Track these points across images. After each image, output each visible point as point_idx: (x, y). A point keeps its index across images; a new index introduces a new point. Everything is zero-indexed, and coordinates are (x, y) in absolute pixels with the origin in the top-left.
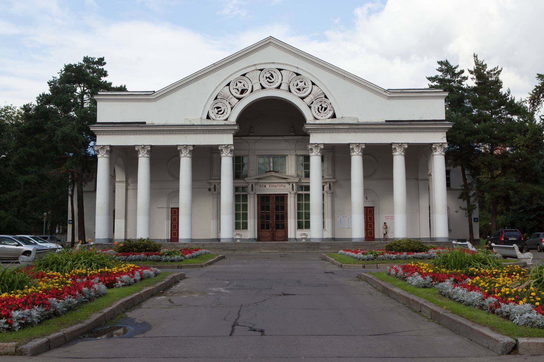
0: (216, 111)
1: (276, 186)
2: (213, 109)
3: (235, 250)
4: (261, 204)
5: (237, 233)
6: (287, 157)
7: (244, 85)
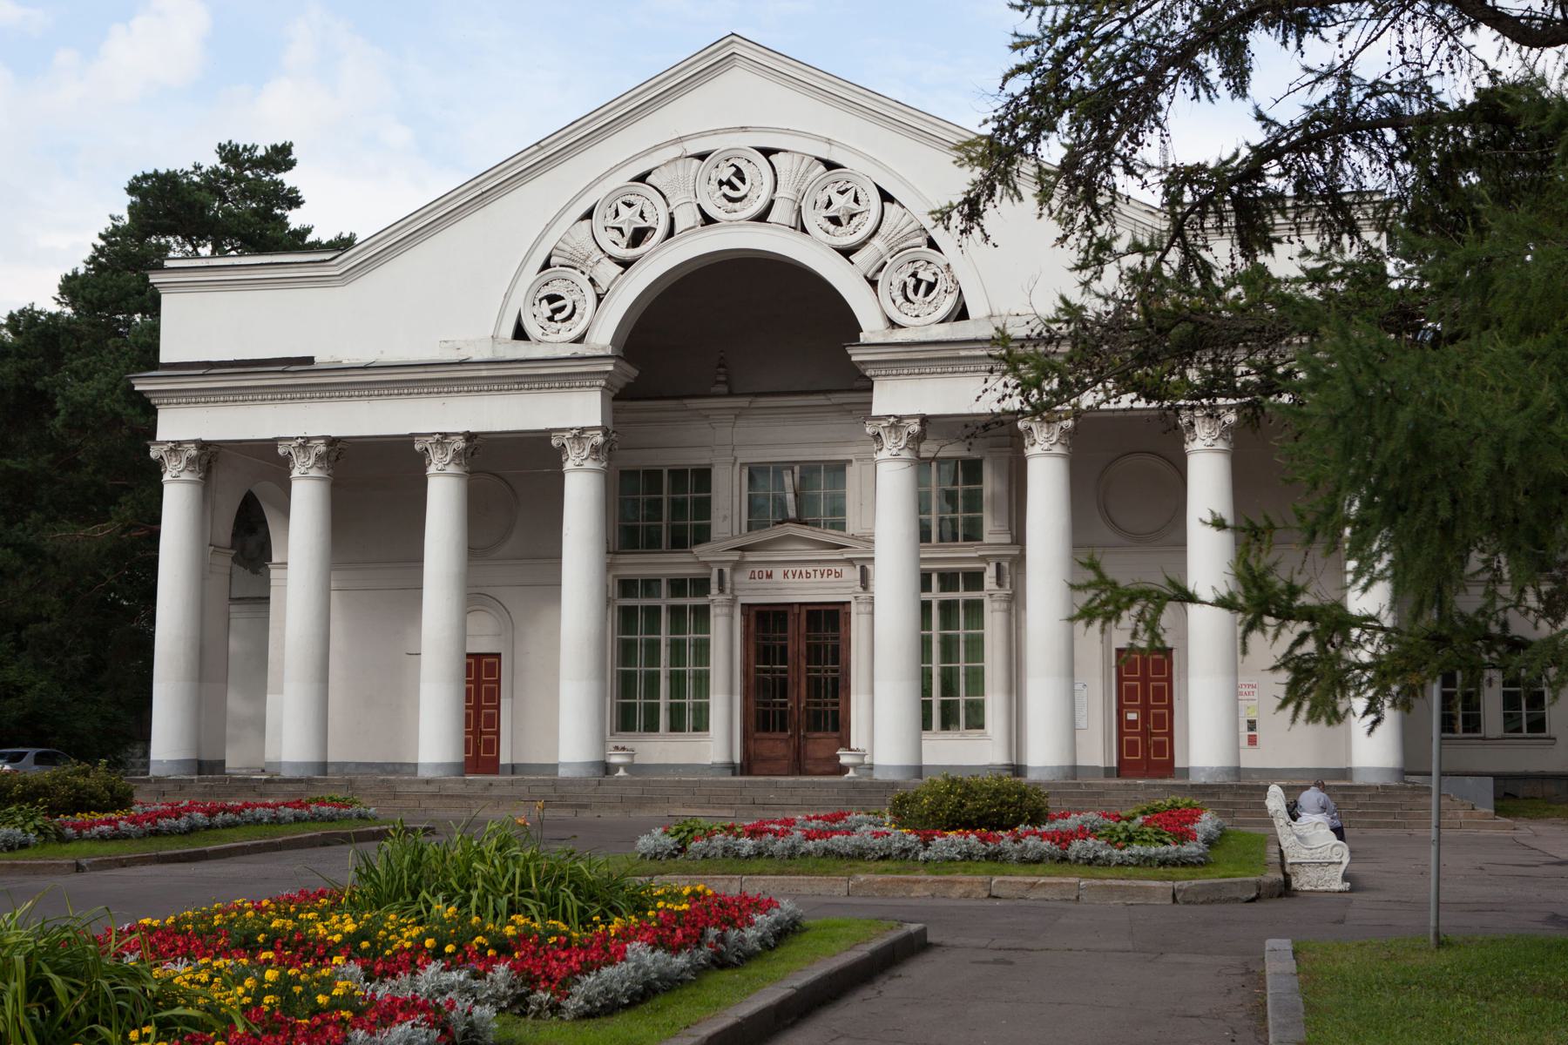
0: (546, 309)
1: (808, 575)
2: (537, 302)
3: (585, 806)
4: (808, 638)
5: (620, 745)
6: (849, 469)
7: (642, 215)
